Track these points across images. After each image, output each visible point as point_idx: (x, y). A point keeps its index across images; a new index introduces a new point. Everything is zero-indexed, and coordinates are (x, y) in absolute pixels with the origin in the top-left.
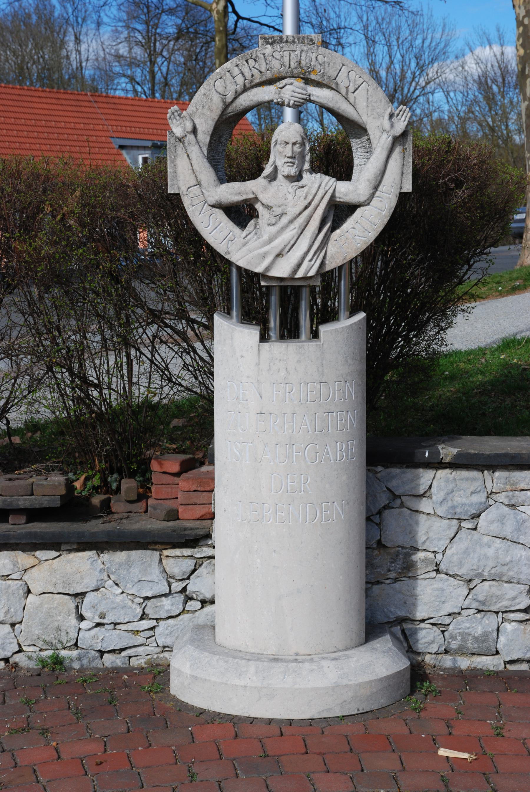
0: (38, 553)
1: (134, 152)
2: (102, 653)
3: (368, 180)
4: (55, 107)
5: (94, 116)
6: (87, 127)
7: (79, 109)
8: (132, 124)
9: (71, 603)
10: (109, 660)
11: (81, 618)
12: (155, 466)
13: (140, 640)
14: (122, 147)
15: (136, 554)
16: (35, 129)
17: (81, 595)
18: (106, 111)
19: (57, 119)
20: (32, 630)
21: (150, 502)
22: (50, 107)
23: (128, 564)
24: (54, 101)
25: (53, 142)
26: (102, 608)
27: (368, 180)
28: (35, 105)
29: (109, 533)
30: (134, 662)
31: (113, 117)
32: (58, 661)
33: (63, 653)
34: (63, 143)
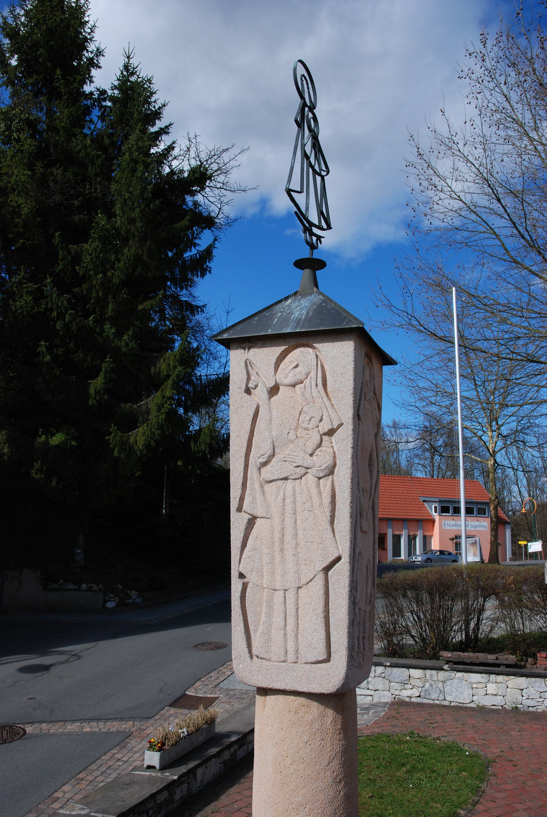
0: (510, 677)
1: (431, 503)
2: (529, 707)
3: (149, 81)
4: (394, 483)
5: (411, 487)
6: (408, 492)
7: (404, 484)
8: (429, 490)
9: (520, 692)
10: (531, 709)
11: (522, 696)
12: (538, 655)
13: (539, 704)
14: (424, 501)
15: (538, 679)
16: (385, 493)
17: (523, 690)
18: (417, 484)
19: (395, 489)
20: (509, 698)
21: (538, 665)
22: (391, 483)
23: (536, 682)
24: (393, 481)
25: (393, 499)
26: (529, 694)
27: (149, 81)
28: (385, 483)
29: (530, 673)
30: (538, 710)
31: (420, 487)
32: (517, 708)
33: (518, 706)
34: (397, 499)
